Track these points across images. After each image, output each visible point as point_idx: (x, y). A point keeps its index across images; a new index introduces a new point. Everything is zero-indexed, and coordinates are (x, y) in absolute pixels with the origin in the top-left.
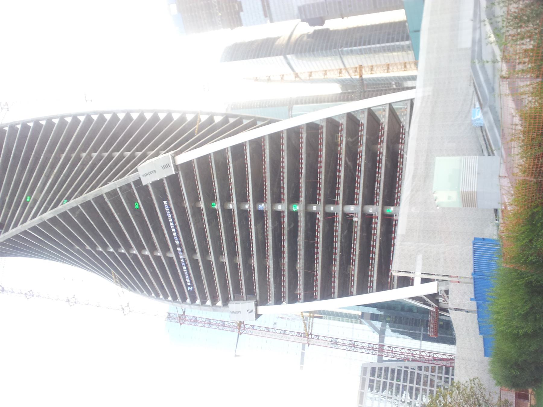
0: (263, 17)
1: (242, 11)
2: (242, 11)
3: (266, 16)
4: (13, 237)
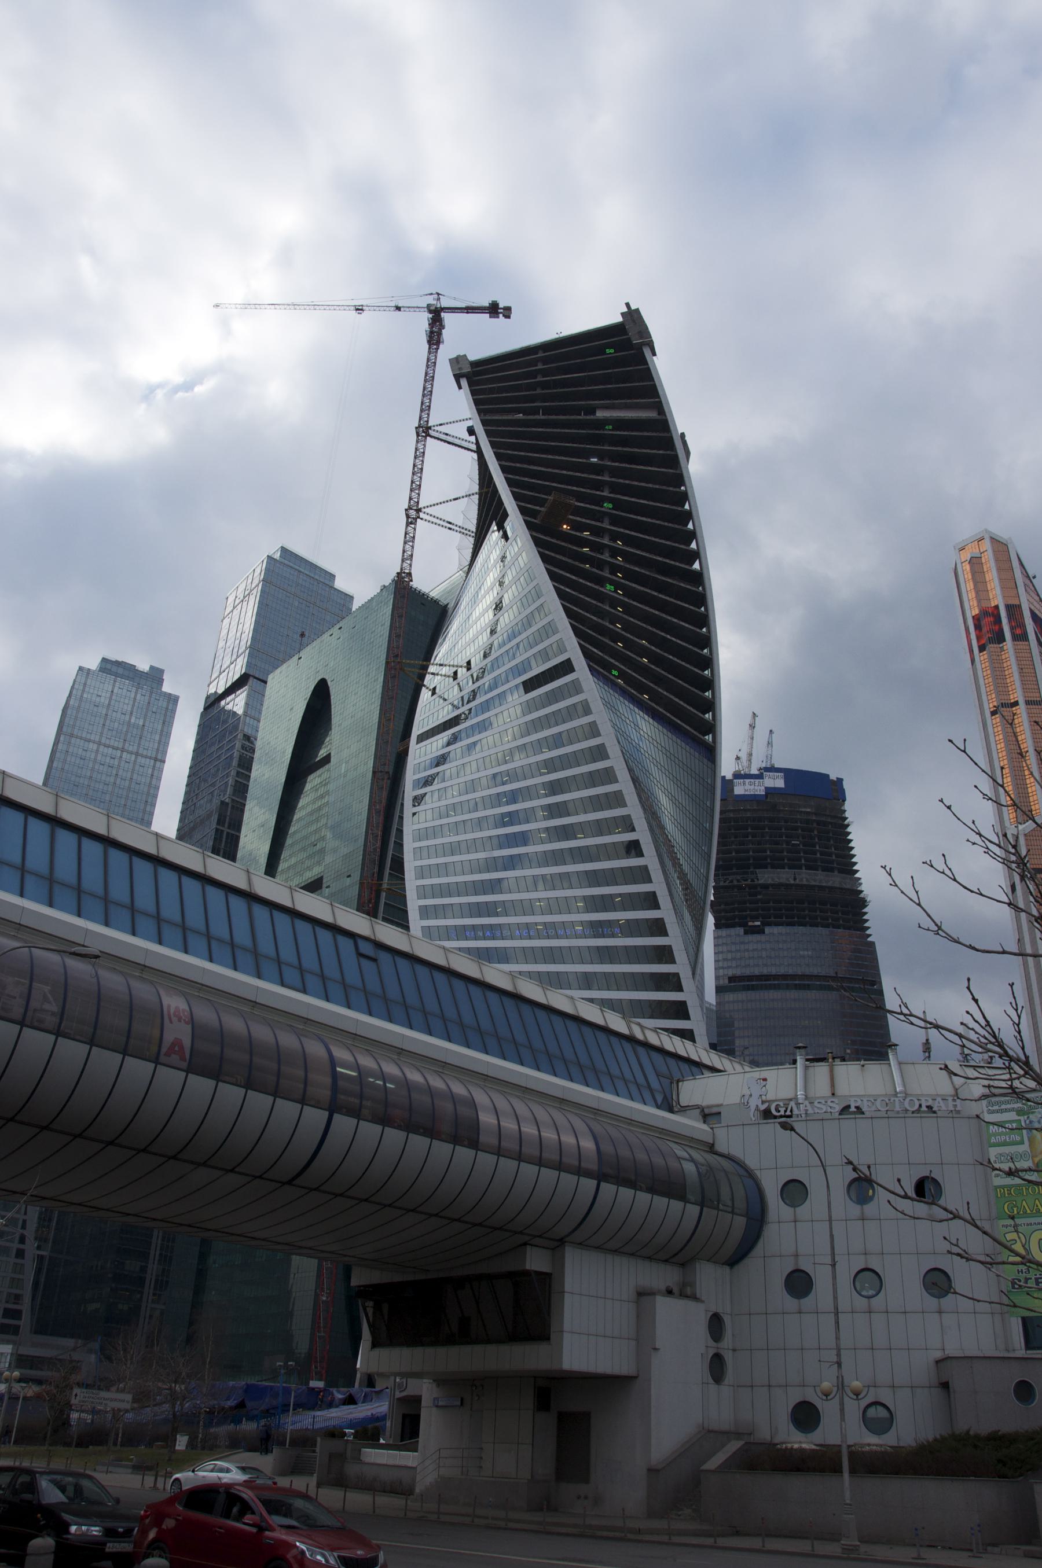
0: (730, 973)
1: (746, 933)
2: (746, 933)
3: (731, 979)
4: (505, 509)
